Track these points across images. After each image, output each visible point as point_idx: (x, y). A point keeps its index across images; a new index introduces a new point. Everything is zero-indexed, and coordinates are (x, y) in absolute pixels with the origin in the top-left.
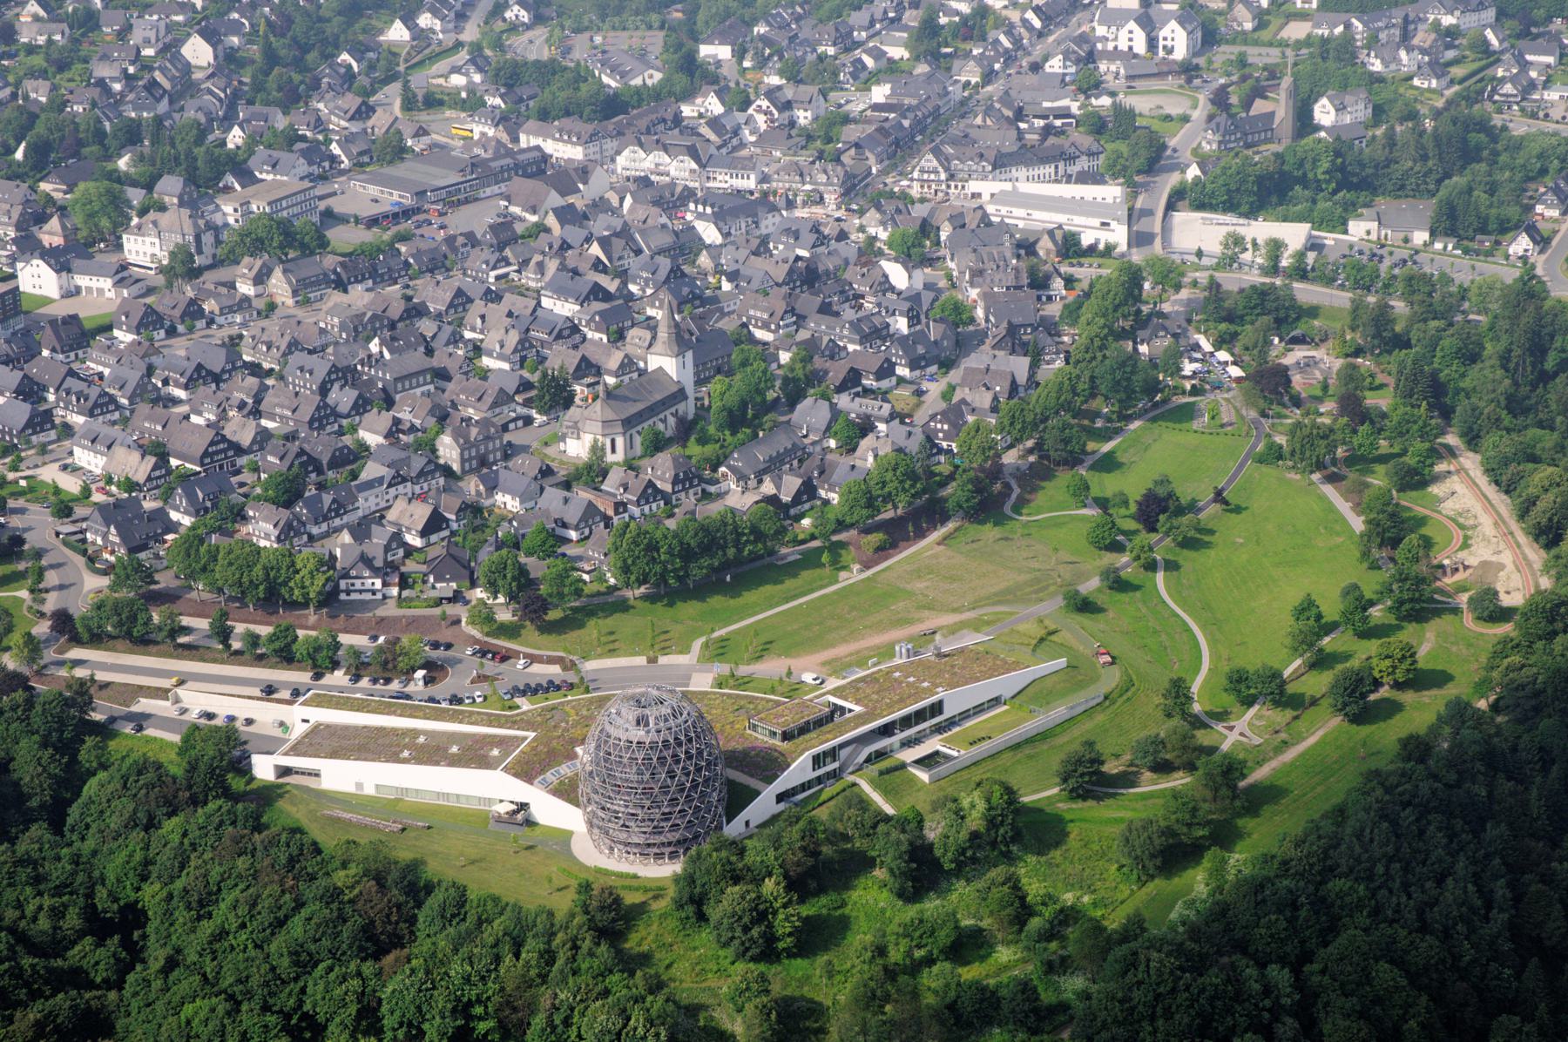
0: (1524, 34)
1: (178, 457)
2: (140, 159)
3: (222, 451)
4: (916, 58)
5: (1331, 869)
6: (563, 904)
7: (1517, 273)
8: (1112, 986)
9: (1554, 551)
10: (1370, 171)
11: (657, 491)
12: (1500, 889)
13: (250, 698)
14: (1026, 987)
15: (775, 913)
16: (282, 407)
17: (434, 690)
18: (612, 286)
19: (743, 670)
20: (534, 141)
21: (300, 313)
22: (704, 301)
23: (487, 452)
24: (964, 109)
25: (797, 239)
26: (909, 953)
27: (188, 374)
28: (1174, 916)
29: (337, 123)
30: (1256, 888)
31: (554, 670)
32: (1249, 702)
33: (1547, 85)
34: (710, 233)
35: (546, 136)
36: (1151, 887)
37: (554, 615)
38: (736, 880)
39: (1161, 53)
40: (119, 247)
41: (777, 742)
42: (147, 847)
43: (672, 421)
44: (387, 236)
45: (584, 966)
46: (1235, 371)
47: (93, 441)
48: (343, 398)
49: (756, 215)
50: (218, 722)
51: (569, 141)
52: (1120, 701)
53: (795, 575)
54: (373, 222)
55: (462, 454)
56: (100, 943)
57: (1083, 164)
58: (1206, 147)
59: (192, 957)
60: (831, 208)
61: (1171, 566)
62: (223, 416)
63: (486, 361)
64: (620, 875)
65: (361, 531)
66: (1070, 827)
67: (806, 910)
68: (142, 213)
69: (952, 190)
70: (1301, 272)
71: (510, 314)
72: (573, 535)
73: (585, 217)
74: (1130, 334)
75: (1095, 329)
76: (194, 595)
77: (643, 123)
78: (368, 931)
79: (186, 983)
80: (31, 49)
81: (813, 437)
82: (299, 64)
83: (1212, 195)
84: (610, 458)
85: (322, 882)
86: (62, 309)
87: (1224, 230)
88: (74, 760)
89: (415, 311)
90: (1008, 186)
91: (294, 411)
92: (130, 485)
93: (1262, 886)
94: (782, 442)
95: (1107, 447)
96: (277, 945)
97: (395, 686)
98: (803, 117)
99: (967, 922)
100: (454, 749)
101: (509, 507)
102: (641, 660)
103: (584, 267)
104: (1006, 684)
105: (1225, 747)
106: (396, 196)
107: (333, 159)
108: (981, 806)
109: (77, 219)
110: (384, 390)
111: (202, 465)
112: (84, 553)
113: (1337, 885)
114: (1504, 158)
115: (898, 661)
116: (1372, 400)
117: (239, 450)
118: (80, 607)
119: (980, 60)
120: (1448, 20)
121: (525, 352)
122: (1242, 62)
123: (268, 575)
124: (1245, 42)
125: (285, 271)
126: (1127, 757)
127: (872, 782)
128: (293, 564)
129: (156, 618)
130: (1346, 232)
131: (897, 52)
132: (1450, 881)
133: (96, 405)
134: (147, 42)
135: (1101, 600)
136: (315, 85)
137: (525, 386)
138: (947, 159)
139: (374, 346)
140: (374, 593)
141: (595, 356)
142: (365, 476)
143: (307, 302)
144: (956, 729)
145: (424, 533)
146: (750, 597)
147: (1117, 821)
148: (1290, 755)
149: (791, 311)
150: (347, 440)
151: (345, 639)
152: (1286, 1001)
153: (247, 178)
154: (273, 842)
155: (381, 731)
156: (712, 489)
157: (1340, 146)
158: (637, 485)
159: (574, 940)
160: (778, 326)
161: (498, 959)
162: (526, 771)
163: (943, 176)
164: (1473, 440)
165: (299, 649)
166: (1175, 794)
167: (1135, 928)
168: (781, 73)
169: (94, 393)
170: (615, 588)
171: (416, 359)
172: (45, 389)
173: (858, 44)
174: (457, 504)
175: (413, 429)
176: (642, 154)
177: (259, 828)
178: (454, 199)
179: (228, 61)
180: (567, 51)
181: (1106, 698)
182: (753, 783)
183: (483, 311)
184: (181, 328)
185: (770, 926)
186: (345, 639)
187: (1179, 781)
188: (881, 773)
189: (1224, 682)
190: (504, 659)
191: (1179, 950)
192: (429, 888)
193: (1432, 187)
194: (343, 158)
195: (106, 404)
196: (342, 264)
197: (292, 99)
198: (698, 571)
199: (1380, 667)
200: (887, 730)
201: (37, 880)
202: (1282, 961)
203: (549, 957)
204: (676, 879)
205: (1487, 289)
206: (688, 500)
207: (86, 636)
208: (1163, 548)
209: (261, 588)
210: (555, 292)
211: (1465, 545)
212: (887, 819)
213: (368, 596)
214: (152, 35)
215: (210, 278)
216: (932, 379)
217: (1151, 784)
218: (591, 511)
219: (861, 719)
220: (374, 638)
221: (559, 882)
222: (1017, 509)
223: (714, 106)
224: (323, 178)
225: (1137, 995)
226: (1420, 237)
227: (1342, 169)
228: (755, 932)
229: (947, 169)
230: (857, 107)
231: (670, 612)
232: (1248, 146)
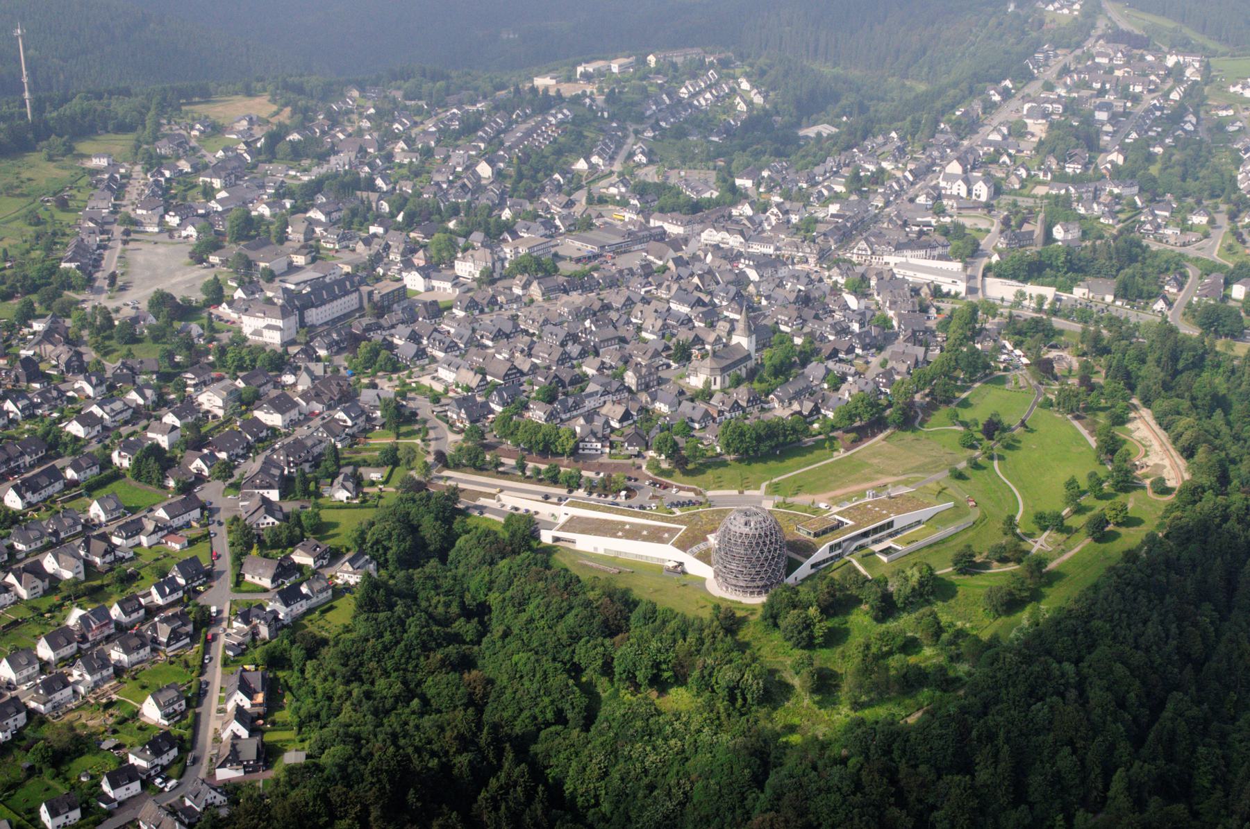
0: (1152, 200)
1: (492, 375)
2: (461, 223)
3: (514, 373)
4: (850, 192)
5: (1092, 615)
6: (706, 614)
7: (1159, 320)
8: (986, 670)
9: (1192, 461)
11: (739, 406)
12: (1173, 629)
14: (941, 669)
17: (630, 501)
18: (707, 299)
19: (789, 500)
20: (658, 223)
21: (546, 305)
22: (754, 310)
24: (876, 219)
26: (880, 649)
28: (1012, 635)
29: (555, 209)
30: (1056, 623)
31: (691, 495)
32: (1044, 529)
33: (1166, 226)
34: (753, 275)
35: (664, 221)
36: (1000, 621)
37: (690, 466)
38: (795, 607)
39: (974, 197)
40: (452, 267)
41: (811, 538)
42: (490, 574)
43: (744, 370)
44: (587, 267)
45: (719, 647)
46: (1025, 361)
48: (574, 349)
50: (521, 512)
53: (811, 452)
54: (578, 260)
56: (468, 621)
57: (939, 251)
58: (1000, 246)
59: (516, 631)
60: (812, 265)
61: (1001, 458)
62: (512, 355)
63: (644, 334)
64: (733, 602)
65: (589, 417)
66: (958, 588)
67: (829, 624)
68: (465, 250)
70: (1054, 312)
71: (656, 311)
72: (697, 426)
73: (688, 263)
74: (972, 338)
75: (957, 335)
76: (504, 446)
77: (714, 217)
78: (605, 622)
79: (514, 645)
80: (401, 166)
81: (816, 382)
82: (534, 178)
84: (713, 388)
85: (581, 597)
86: (429, 298)
87: (1015, 289)
88: (450, 528)
89: (607, 307)
90: (904, 260)
92: (469, 389)
93: (1059, 623)
94: (801, 384)
95: (964, 395)
96: (560, 628)
97: (610, 498)
98: (794, 219)
99: (910, 634)
100: (645, 533)
102: (735, 492)
103: (690, 289)
104: (924, 513)
105: (1034, 551)
106: (589, 247)
107: (557, 228)
108: (917, 575)
109: (433, 251)
112: (447, 422)
113: (1097, 623)
114: (1149, 261)
115: (867, 500)
116: (1095, 379)
117: (522, 374)
118: (449, 450)
119: (883, 194)
120: (1116, 191)
121: (664, 332)
122: (1015, 204)
124: (1016, 195)
126: (985, 554)
127: (858, 560)
129: (488, 458)
131: (840, 189)
132: (1150, 624)
134: (459, 164)
135: (968, 473)
136: (543, 190)
137: (667, 348)
139: (587, 323)
141: (702, 335)
142: (588, 390)
143: (549, 299)
145: (621, 421)
146: (789, 462)
147: (982, 586)
148: (1066, 557)
149: (800, 317)
150: (577, 370)
151: (584, 473)
152: (1072, 681)
153: (515, 235)
154: (557, 575)
156: (766, 406)
157: (1069, 250)
158: (730, 402)
159: (714, 633)
161: (675, 641)
162: (683, 545)
164: (1147, 402)
165: (561, 477)
166: (1013, 574)
167: (994, 641)
168: (781, 195)
169: (448, 341)
170: (720, 454)
171: (610, 332)
172: (421, 337)
173: (818, 183)
174: (637, 407)
175: (611, 367)
177: (548, 567)
178: (619, 251)
179: (499, 175)
180: (667, 178)
182: (799, 558)
184: (486, 310)
186: (584, 473)
187: (1012, 567)
188: (863, 556)
189: (1032, 518)
190: (665, 488)
191: (1019, 653)
192: (636, 604)
197: (532, 196)
198: (764, 448)
199: (1109, 514)
200: (865, 535)
201: (437, 587)
202: (1068, 660)
203: (701, 641)
204: (764, 605)
205: (1149, 325)
206: (755, 411)
208: (997, 448)
211: (1146, 455)
212: (866, 580)
214: (461, 161)
215: (500, 285)
216: (873, 355)
217: (997, 569)
218: (706, 414)
219: (852, 528)
220: (598, 474)
221: (702, 603)
222: (921, 424)
223: (747, 210)
224: (551, 236)
225: (999, 675)
226: (1109, 298)
228: (804, 634)
230: (821, 215)
232: (1021, 247)
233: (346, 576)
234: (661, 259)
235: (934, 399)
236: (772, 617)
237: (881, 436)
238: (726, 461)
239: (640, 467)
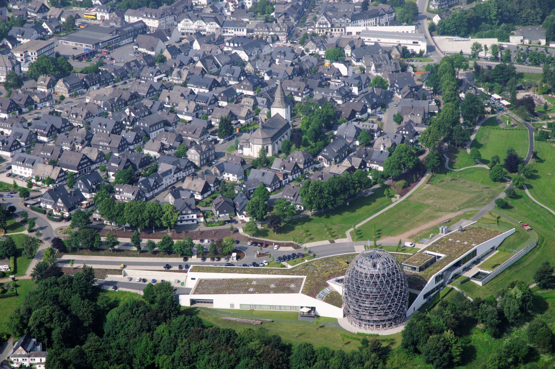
10: (512, 15)
11: (298, 168)
13: (160, 271)
15: (451, 346)
16: (103, 141)
17: (242, 261)
23: (209, 156)
25: (285, 56)
27: (48, 129)
38: (431, 333)
46: (505, 103)
47: (23, 162)
49: (260, 47)
51: (151, 18)
52: (543, 245)
55: (200, 157)
57: (386, 18)
61: (529, 187)
69: (334, 32)
83: (449, 28)
91: (110, 143)
97: (223, 260)
100: (273, 286)
101: (231, 179)
102: (327, 242)
104: (496, 241)
106: (84, 46)
107: (45, 30)
110: (144, 130)
111: (78, 170)
112: (45, 212)
117: (93, 163)
123: (150, 215)
125: (64, 81)
128: (161, 209)
130: (509, 41)
133: (12, 146)
138: (330, 18)
140: (193, 220)
144: (482, 262)
145: (202, 193)
146: (360, 211)
160: (303, 94)
162: (312, 292)
163: (329, 26)
175: (171, 148)
176: (191, 22)
181: (537, 244)
183: (168, 94)
185: (450, 352)
190: (267, 246)
193: (539, 20)
194: (49, 30)
195: (16, 145)
196: (87, 77)
200: (457, 265)
207: (70, 249)
209: (147, 221)
210: (194, 84)
213: (190, 222)
216: (381, 113)
219: (449, 259)
228: (445, 355)
229: (331, 23)
231: (328, 220)
233: (20, 359)
234: (152, 49)
235: (453, 143)
237: (424, 180)
238: (308, 216)
239: (237, 231)
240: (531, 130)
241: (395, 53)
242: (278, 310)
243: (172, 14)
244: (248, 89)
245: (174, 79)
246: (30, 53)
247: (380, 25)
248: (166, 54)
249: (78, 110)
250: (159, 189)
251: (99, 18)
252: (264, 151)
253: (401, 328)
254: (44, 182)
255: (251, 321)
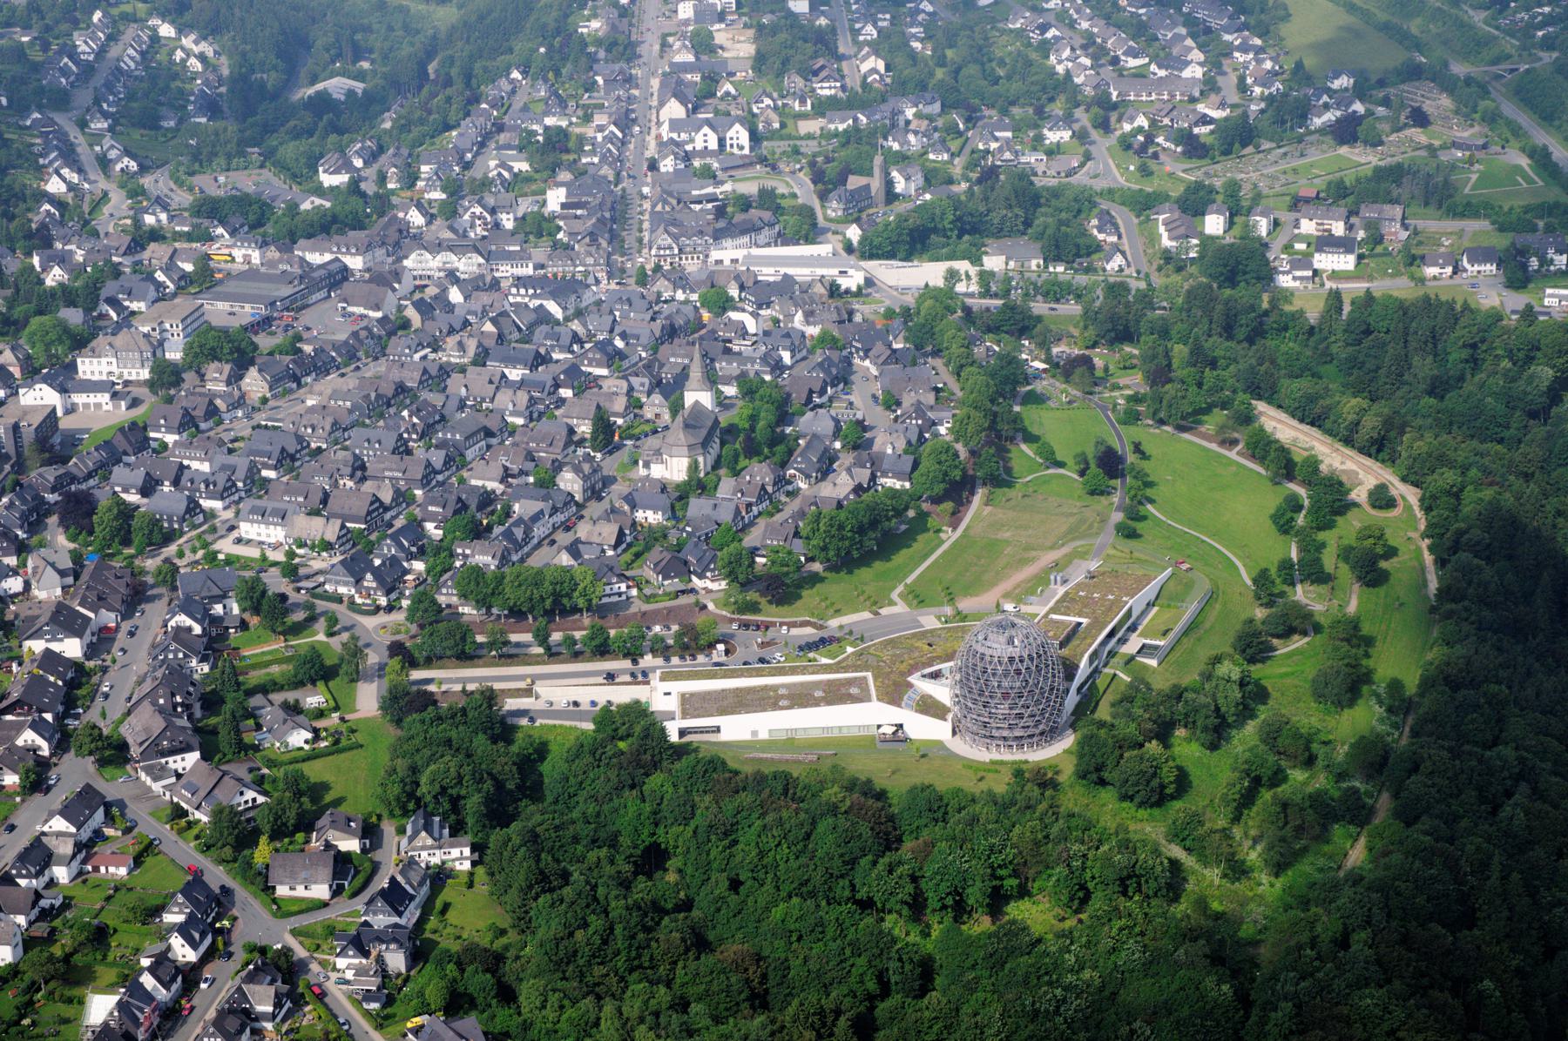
16: (391, 470)
27: (276, 454)
102: (866, 615)
104: (1149, 591)
106: (248, 308)
125: (260, 371)
128: (572, 578)
133: (226, 489)
140: (620, 594)
144: (1140, 628)
145: (615, 547)
155: (765, 688)
162: (894, 693)
176: (428, 256)
194: (168, 283)
196: (294, 361)
200: (1111, 634)
207: (422, 661)
210: (501, 361)
213: (615, 599)
219: (1097, 624)
227: (959, 219)
233: (424, 854)
234: (377, 308)
236: (1093, 772)
237: (978, 499)
239: (704, 607)
240: (1104, 409)
241: (820, 290)
242: (836, 734)
243: (383, 243)
244: (599, 365)
245: (451, 355)
246: (167, 326)
247: (758, 246)
248: (411, 313)
249: (315, 419)
250: (530, 546)
251: (239, 259)
252: (693, 467)
253: (1068, 741)
254: (312, 548)
255: (801, 757)
